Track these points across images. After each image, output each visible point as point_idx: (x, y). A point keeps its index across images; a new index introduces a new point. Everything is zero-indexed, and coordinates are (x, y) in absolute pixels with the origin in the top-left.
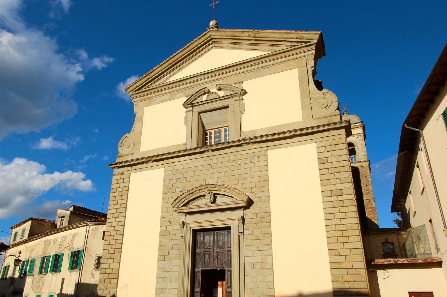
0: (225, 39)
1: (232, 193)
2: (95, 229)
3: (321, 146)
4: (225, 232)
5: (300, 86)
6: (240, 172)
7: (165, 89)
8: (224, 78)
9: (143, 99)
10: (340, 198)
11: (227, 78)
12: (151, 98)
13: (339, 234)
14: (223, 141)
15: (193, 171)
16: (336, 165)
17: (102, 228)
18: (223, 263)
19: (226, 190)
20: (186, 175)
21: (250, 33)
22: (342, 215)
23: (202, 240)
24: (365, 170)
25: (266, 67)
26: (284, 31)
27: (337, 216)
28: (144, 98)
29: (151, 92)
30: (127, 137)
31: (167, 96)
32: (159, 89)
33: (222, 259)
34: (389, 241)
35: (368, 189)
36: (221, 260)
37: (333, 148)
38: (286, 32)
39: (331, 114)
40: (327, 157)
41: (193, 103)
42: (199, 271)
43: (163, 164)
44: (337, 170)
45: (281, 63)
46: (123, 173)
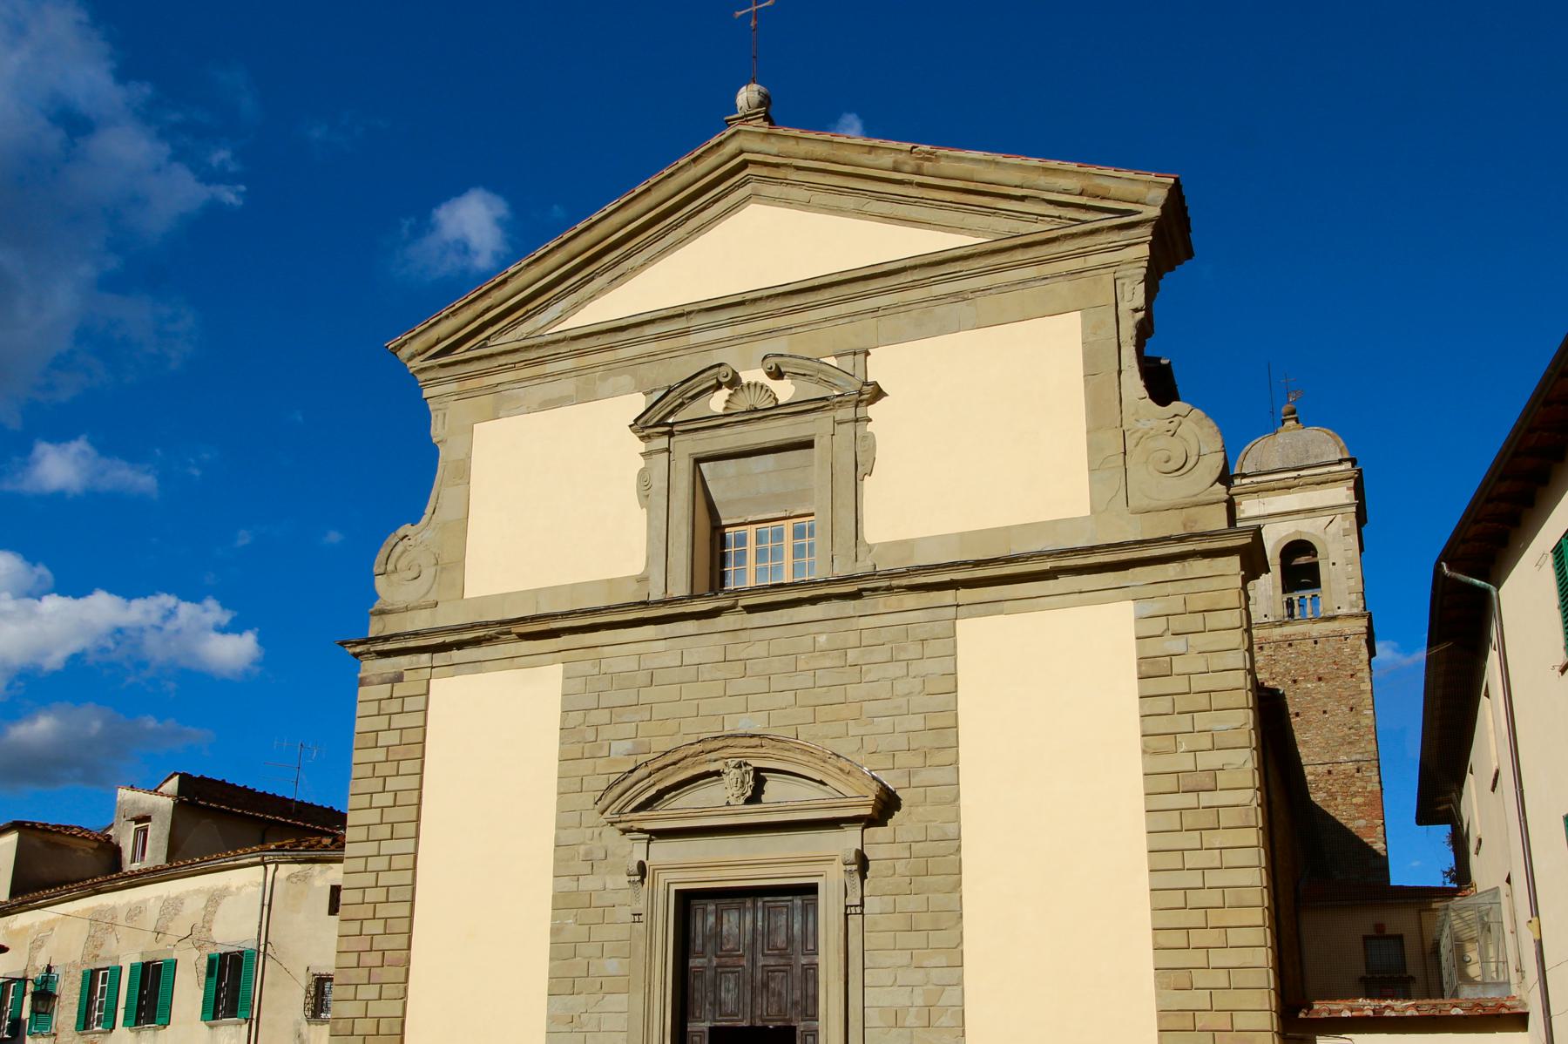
1: (822, 769)
5: (1085, 381)
6: (854, 692)
7: (557, 357)
8: (793, 331)
9: (466, 391)
10: (1206, 799)
13: (1196, 918)
15: (677, 680)
16: (1199, 683)
17: (326, 876)
18: (789, 1005)
19: (799, 757)
20: (648, 695)
21: (901, 157)
22: (1213, 858)
23: (710, 927)
24: (1352, 650)
25: (959, 296)
27: (1192, 859)
28: (470, 384)
29: (501, 363)
30: (407, 536)
31: (567, 386)
32: (533, 354)
34: (1388, 932)
35: (1359, 723)
37: (1196, 622)
39: (1194, 499)
41: (670, 421)
44: (1202, 701)
45: (1020, 286)
46: (399, 678)
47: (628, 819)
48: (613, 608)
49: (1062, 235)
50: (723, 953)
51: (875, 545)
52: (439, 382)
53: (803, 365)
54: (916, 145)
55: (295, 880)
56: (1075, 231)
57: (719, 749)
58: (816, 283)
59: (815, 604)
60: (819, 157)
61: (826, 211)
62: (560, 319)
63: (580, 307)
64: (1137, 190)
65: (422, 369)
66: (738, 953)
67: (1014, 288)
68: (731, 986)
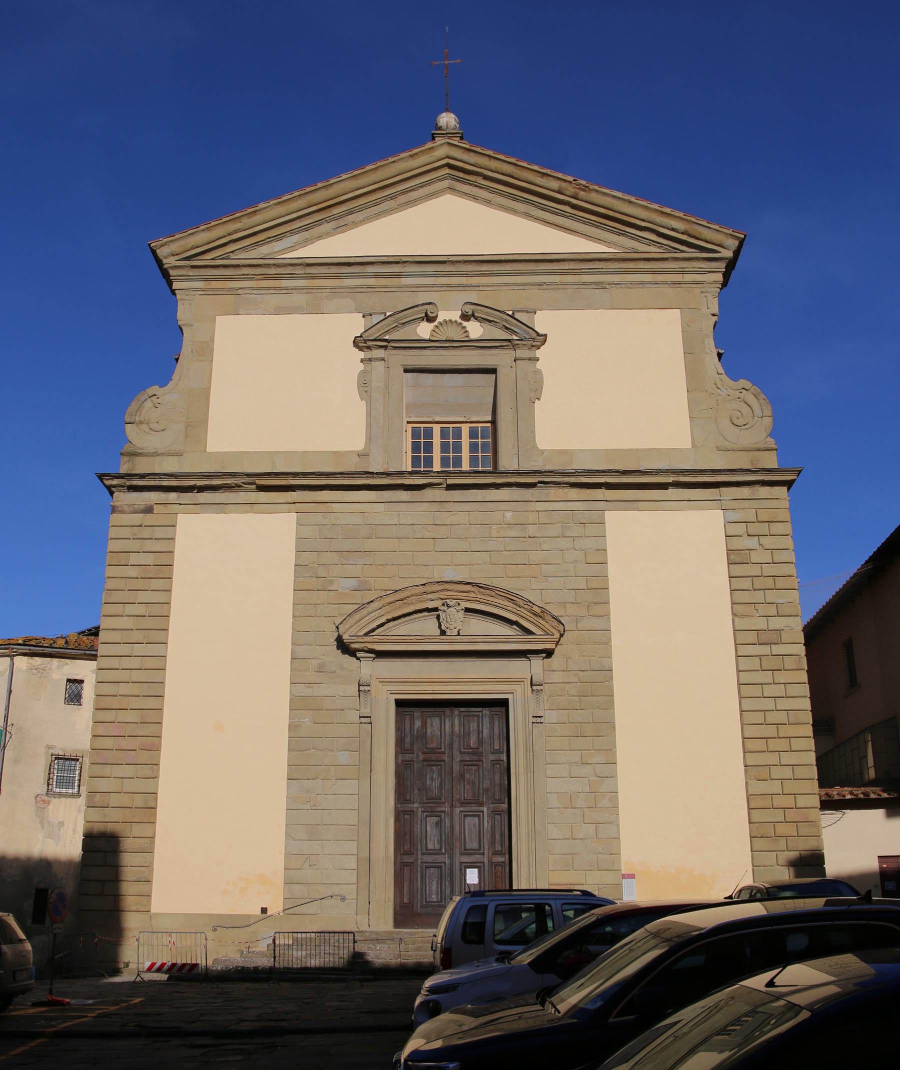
0: (486, 178)
2: (37, 669)
3: (736, 520)
4: (484, 712)
7: (292, 277)
8: (481, 288)
9: (212, 290)
10: (776, 649)
11: (491, 289)
12: (240, 292)
13: (771, 731)
14: (466, 467)
16: (769, 570)
18: (481, 791)
20: (370, 545)
21: (564, 185)
22: (779, 690)
23: (418, 730)
25: (599, 285)
26: (655, 206)
27: (769, 691)
28: (214, 284)
32: (273, 271)
33: (477, 781)
36: (474, 783)
37: (763, 528)
38: (660, 209)
40: (749, 548)
42: (411, 809)
43: (294, 503)
44: (769, 583)
45: (640, 286)
47: (363, 641)
48: (347, 474)
49: (670, 258)
50: (428, 750)
51: (544, 450)
52: (188, 279)
53: (492, 314)
54: (576, 179)
55: (35, 672)
56: (680, 256)
57: (438, 591)
58: (503, 258)
59: (498, 489)
60: (504, 172)
61: (502, 209)
62: (292, 248)
63: (310, 242)
64: (719, 238)
65: (176, 266)
66: (440, 750)
67: (637, 286)
68: (434, 776)
